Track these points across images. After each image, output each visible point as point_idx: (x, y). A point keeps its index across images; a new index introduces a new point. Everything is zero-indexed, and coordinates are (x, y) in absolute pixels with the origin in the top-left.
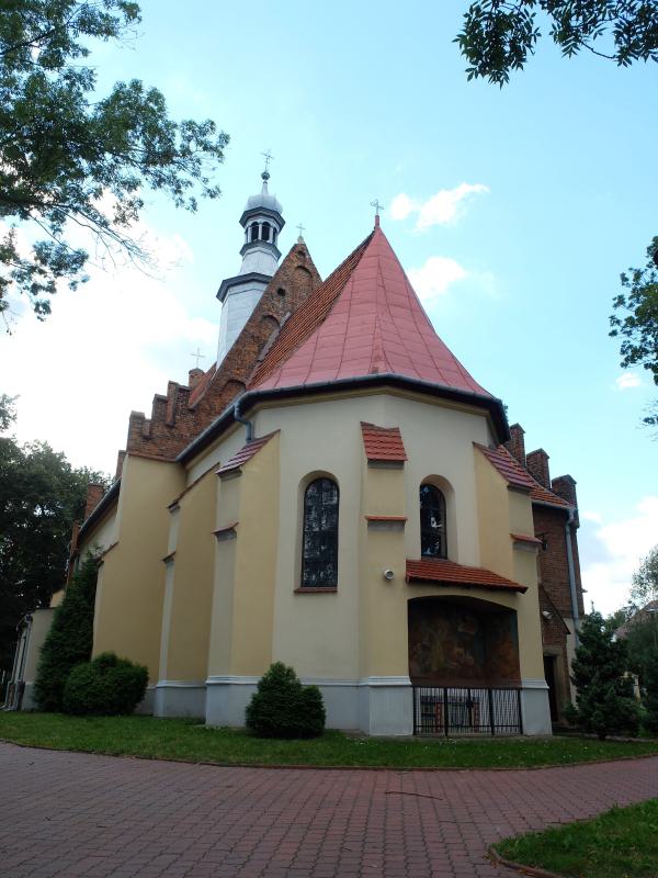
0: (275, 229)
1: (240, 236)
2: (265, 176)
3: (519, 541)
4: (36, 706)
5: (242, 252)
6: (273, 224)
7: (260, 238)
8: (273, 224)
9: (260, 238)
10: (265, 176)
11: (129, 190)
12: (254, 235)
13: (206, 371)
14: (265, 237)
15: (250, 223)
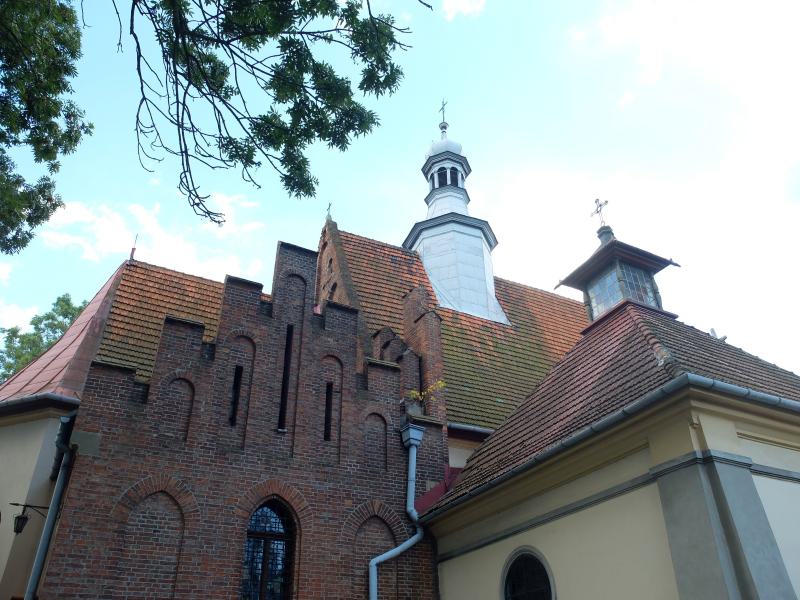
2: (444, 127)
5: (427, 200)
7: (449, 182)
9: (449, 182)
10: (444, 127)
12: (443, 183)
13: (399, 244)
15: (436, 168)
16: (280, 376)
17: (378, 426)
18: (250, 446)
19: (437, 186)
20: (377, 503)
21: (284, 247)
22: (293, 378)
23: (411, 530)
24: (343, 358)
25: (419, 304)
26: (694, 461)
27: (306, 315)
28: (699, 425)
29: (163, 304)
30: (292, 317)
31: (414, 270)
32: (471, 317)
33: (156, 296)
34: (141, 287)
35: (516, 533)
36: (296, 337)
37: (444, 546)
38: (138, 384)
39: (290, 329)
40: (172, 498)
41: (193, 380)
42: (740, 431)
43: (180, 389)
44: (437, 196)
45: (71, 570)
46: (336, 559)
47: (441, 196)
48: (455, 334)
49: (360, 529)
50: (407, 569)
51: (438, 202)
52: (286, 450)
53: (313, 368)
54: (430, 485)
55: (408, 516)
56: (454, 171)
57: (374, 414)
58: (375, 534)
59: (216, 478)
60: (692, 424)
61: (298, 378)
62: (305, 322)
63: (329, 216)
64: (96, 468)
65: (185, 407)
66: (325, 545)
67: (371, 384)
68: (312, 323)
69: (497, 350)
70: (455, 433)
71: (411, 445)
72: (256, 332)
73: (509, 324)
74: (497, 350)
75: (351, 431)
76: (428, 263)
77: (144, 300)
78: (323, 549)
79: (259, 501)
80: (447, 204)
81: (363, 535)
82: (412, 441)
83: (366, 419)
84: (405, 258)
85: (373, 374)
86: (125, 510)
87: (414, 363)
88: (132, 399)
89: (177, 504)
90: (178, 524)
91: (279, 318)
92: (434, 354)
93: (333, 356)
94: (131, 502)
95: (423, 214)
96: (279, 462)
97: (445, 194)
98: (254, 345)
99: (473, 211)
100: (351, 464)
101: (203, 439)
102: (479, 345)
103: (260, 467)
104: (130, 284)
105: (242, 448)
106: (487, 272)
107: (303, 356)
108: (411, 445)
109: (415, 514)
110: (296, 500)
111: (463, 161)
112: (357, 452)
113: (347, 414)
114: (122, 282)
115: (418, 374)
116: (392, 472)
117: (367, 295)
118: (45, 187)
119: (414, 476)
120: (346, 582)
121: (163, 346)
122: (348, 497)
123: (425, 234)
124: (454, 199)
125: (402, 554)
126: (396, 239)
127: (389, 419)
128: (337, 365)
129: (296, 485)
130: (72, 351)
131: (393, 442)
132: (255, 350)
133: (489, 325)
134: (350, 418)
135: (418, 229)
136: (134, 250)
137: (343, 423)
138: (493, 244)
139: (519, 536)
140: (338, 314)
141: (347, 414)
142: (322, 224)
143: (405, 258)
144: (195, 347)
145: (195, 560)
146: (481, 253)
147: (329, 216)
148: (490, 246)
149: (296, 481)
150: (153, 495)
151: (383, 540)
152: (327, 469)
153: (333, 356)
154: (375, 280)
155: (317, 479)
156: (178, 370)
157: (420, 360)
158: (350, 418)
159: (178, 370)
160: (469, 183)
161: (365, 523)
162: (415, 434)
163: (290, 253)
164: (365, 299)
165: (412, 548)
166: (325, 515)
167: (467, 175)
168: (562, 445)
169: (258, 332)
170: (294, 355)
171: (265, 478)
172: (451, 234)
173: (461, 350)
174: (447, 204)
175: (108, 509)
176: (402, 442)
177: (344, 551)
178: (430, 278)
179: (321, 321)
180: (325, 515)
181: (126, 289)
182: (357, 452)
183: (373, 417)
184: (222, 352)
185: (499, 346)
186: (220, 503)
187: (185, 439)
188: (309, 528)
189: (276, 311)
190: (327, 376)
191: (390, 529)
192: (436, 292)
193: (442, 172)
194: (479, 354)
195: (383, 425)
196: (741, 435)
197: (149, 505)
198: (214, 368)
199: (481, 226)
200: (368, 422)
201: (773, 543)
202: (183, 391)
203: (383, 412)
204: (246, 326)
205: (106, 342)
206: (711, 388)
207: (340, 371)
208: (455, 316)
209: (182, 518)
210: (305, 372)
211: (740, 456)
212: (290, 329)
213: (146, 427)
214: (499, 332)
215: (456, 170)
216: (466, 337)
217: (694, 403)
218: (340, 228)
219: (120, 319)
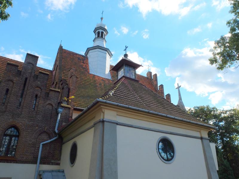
2: (102, 19)
5: (94, 41)
7: (100, 36)
9: (100, 36)
10: (102, 19)
12: (98, 36)
15: (97, 31)
17: (50, 107)
18: (8, 111)
19: (97, 37)
20: (46, 128)
21: (28, 55)
23: (55, 136)
24: (42, 88)
27: (32, 75)
28: (104, 112)
29: (2, 68)
31: (85, 62)
32: (99, 77)
35: (73, 138)
36: (28, 81)
37: (65, 140)
39: (26, 79)
42: (117, 114)
44: (96, 40)
46: (30, 143)
47: (98, 40)
48: (92, 80)
49: (40, 135)
54: (64, 124)
55: (55, 132)
56: (102, 33)
57: (49, 104)
60: (102, 112)
61: (26, 93)
63: (61, 44)
71: (59, 113)
73: (111, 79)
76: (90, 60)
78: (27, 140)
79: (8, 127)
80: (99, 43)
81: (40, 136)
83: (47, 105)
84: (84, 59)
85: (51, 93)
87: (67, 90)
92: (73, 88)
93: (39, 87)
95: (92, 45)
96: (16, 116)
98: (13, 83)
102: (99, 85)
105: (5, 112)
107: (29, 87)
109: (57, 131)
111: (105, 30)
112: (42, 114)
113: (40, 104)
115: (68, 93)
117: (66, 69)
119: (58, 121)
122: (37, 126)
123: (90, 51)
125: (51, 142)
126: (83, 53)
127: (54, 105)
128: (40, 90)
129: (21, 122)
132: (13, 84)
133: (104, 79)
134: (41, 105)
135: (88, 50)
139: (73, 140)
140: (42, 75)
143: (84, 59)
147: (61, 44)
148: (110, 56)
149: (21, 121)
151: (46, 138)
153: (39, 87)
154: (71, 64)
155: (28, 121)
157: (69, 89)
158: (41, 105)
161: (41, 133)
166: (29, 131)
169: (15, 79)
171: (11, 120)
173: (92, 86)
174: (99, 43)
176: (57, 112)
178: (89, 65)
180: (29, 131)
183: (49, 105)
185: (105, 85)
189: (22, 74)
191: (49, 136)
192: (90, 69)
193: (99, 33)
195: (52, 107)
199: (106, 50)
200: (47, 106)
203: (52, 103)
206: (105, 103)
210: (29, 91)
212: (26, 79)
214: (107, 82)
215: (103, 32)
216: (95, 82)
217: (102, 106)
218: (63, 48)
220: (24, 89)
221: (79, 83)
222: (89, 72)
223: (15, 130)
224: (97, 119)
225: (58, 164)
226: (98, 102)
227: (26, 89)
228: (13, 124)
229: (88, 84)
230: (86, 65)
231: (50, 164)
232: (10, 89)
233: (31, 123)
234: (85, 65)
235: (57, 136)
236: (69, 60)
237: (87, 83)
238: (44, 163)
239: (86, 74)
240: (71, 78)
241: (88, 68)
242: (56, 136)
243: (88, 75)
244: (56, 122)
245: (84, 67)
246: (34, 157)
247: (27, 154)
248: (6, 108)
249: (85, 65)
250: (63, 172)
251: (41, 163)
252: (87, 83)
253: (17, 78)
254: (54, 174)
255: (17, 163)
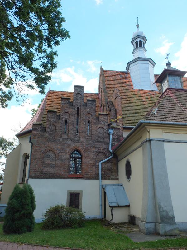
0: (144, 42)
1: (132, 47)
2: (138, 26)
3: (146, 139)
4: (147, 129)
5: (133, 53)
6: (143, 40)
7: (139, 46)
8: (143, 40)
9: (139, 46)
10: (138, 26)
11: (47, 66)
12: (137, 47)
13: (84, 92)
14: (141, 45)
15: (135, 42)
16: (76, 121)
17: (102, 130)
19: (135, 48)
22: (79, 121)
24: (92, 113)
25: (117, 94)
26: (147, 141)
30: (78, 105)
31: (127, 78)
32: (144, 90)
33: (56, 99)
34: (52, 97)
35: (126, 156)
36: (79, 110)
38: (43, 127)
39: (78, 108)
40: (53, 151)
41: (55, 125)
43: (53, 127)
45: (34, 167)
46: (91, 162)
49: (97, 155)
50: (110, 164)
51: (135, 53)
52: (78, 138)
53: (84, 118)
54: (116, 143)
55: (110, 151)
57: (101, 127)
58: (101, 156)
59: (62, 146)
62: (82, 106)
63: (101, 66)
64: (37, 146)
65: (54, 131)
66: (88, 159)
67: (100, 119)
68: (84, 106)
69: (151, 100)
70: (124, 128)
72: (69, 111)
74: (151, 100)
75: (94, 132)
77: (53, 101)
81: (98, 156)
82: (110, 133)
83: (99, 129)
84: (125, 75)
85: (100, 117)
86: (44, 155)
87: (114, 111)
88: (43, 131)
89: (54, 152)
90: (55, 157)
91: (75, 106)
94: (45, 153)
95: (131, 58)
96: (77, 141)
97: (137, 51)
98: (69, 114)
99: (147, 55)
100: (95, 140)
101: (59, 138)
102: (145, 99)
103: (72, 143)
104: (50, 97)
106: (150, 73)
108: (110, 134)
109: (111, 151)
110: (81, 150)
111: (143, 37)
112: (96, 137)
113: (93, 128)
114: (48, 97)
116: (106, 141)
118: (10, 92)
120: (94, 167)
121: (48, 118)
122: (94, 148)
123: (131, 65)
124: (140, 52)
125: (108, 161)
126: (122, 68)
127: (105, 128)
128: (91, 115)
130: (37, 118)
131: (106, 133)
134: (94, 129)
135: (129, 64)
136: (50, 87)
137: (92, 130)
138: (154, 64)
140: (90, 102)
141: (93, 128)
142: (100, 69)
144: (55, 117)
145: (59, 164)
146: (148, 69)
147: (101, 66)
148: (153, 65)
150: (49, 151)
152: (89, 142)
156: (51, 123)
157: (116, 110)
158: (94, 129)
159: (51, 123)
160: (146, 46)
162: (111, 131)
163: (77, 88)
164: (110, 91)
165: (111, 159)
166: (88, 152)
167: (146, 41)
168: (185, 124)
170: (79, 115)
171: (73, 145)
172: (138, 64)
174: (140, 54)
175: (40, 155)
177: (93, 160)
178: (132, 80)
179: (86, 105)
180: (88, 152)
181: (49, 99)
182: (96, 137)
183: (101, 128)
184: (61, 117)
186: (63, 151)
187: (55, 138)
188: (84, 155)
189: (74, 105)
190: (88, 119)
191: (105, 155)
192: (133, 84)
193: (137, 43)
194: (144, 102)
196: (163, 132)
197: (48, 153)
198: (60, 121)
199: (148, 60)
200: (99, 129)
201: (164, 159)
202: (53, 127)
203: (103, 126)
204: (67, 110)
205: (45, 114)
206: (149, 123)
207: (91, 117)
208: (139, 91)
209: (56, 155)
211: (160, 139)
212: (78, 108)
213: (46, 137)
217: (146, 127)
219: (48, 107)
220: (78, 118)
221: (124, 101)
222: (133, 88)
223: (78, 153)
224: (144, 139)
225: (117, 179)
226: (142, 123)
227: (79, 117)
228: (75, 148)
229: (134, 100)
230: (129, 81)
231: (110, 180)
232: (68, 120)
233: (89, 146)
234: (128, 81)
235: (112, 155)
236: (111, 80)
237: (132, 100)
238: (105, 179)
239: (130, 91)
240: (116, 99)
241: (131, 84)
242: (111, 155)
243: (132, 91)
244: (109, 143)
245: (127, 83)
246: (96, 174)
247: (90, 172)
248: (68, 136)
249: (128, 81)
250: (122, 185)
251: (102, 179)
252: (132, 100)
253: (71, 109)
254: (114, 187)
255: (84, 179)
